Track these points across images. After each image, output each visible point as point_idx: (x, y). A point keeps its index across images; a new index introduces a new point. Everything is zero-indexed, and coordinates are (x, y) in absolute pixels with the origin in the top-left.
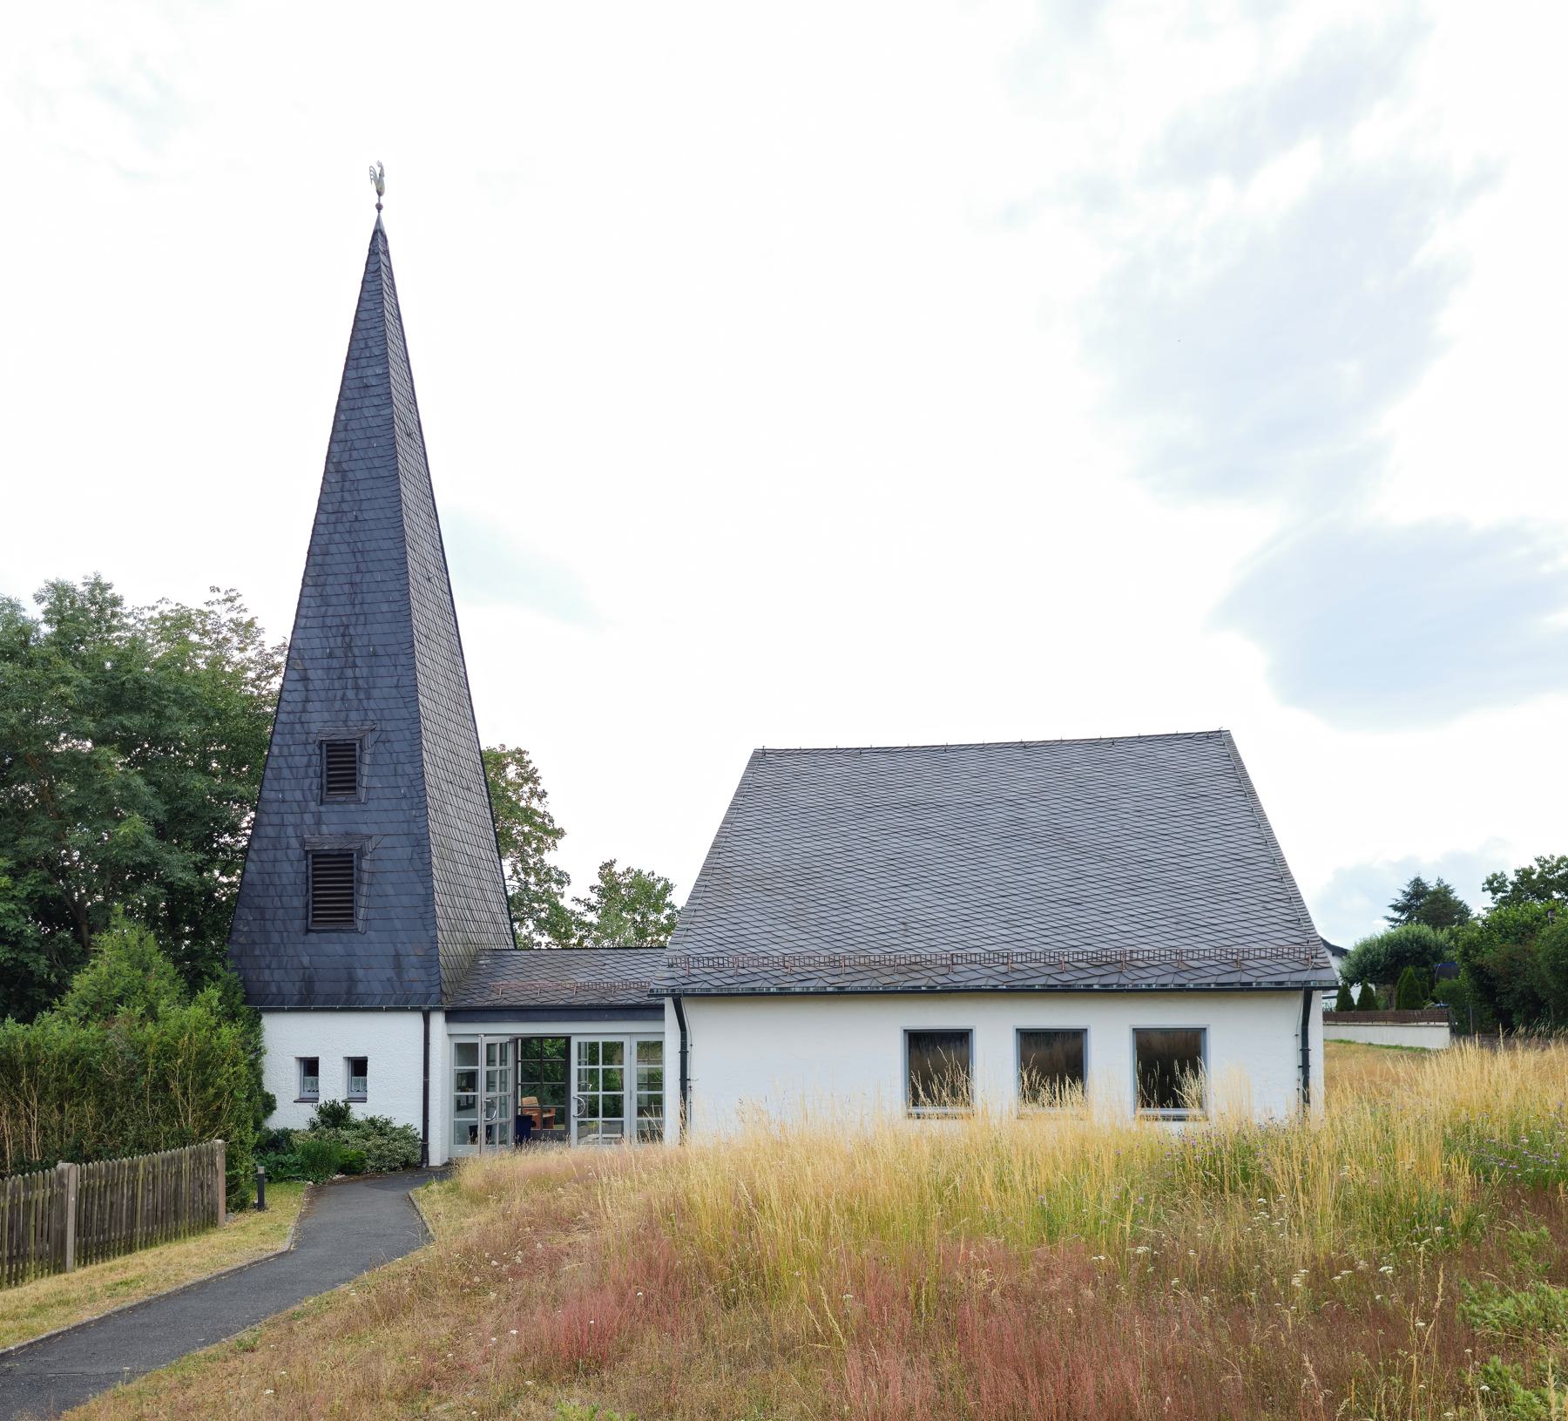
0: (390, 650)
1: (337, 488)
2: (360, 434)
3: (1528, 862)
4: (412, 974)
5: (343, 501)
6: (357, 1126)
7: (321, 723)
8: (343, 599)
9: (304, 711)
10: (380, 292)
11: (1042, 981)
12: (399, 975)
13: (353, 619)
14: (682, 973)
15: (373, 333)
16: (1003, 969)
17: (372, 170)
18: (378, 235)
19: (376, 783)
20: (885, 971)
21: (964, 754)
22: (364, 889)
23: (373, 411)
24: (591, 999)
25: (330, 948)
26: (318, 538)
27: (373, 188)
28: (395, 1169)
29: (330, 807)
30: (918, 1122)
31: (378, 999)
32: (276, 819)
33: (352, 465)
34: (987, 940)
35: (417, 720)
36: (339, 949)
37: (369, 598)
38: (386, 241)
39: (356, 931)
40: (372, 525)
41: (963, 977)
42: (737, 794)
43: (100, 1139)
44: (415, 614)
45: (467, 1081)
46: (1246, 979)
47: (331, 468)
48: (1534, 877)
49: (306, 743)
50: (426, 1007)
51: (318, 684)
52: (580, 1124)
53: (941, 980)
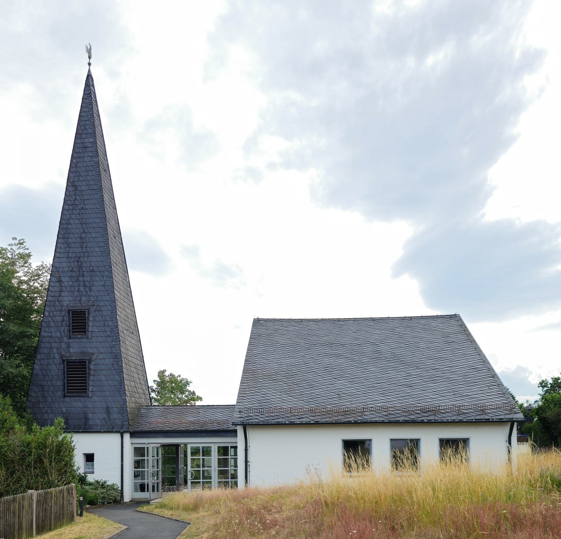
1: (72, 193)
2: (83, 169)
4: (115, 416)
6: (91, 484)
7: (68, 301)
8: (77, 245)
9: (60, 296)
10: (91, 104)
11: (403, 418)
12: (109, 417)
13: (82, 254)
14: (246, 415)
15: (88, 123)
17: (87, 47)
18: (89, 77)
19: (95, 329)
21: (347, 322)
22: (91, 378)
23: (89, 159)
24: (215, 427)
25: (76, 404)
26: (64, 216)
27: (87, 55)
28: (109, 503)
29: (73, 340)
31: (99, 427)
32: (48, 345)
33: (80, 183)
35: (114, 301)
38: (93, 80)
39: (88, 396)
40: (90, 211)
41: (368, 417)
42: (251, 338)
43: (8, 485)
44: (111, 253)
46: (487, 417)
47: (70, 184)
50: (122, 431)
51: (66, 284)
52: (192, 483)
53: (360, 418)
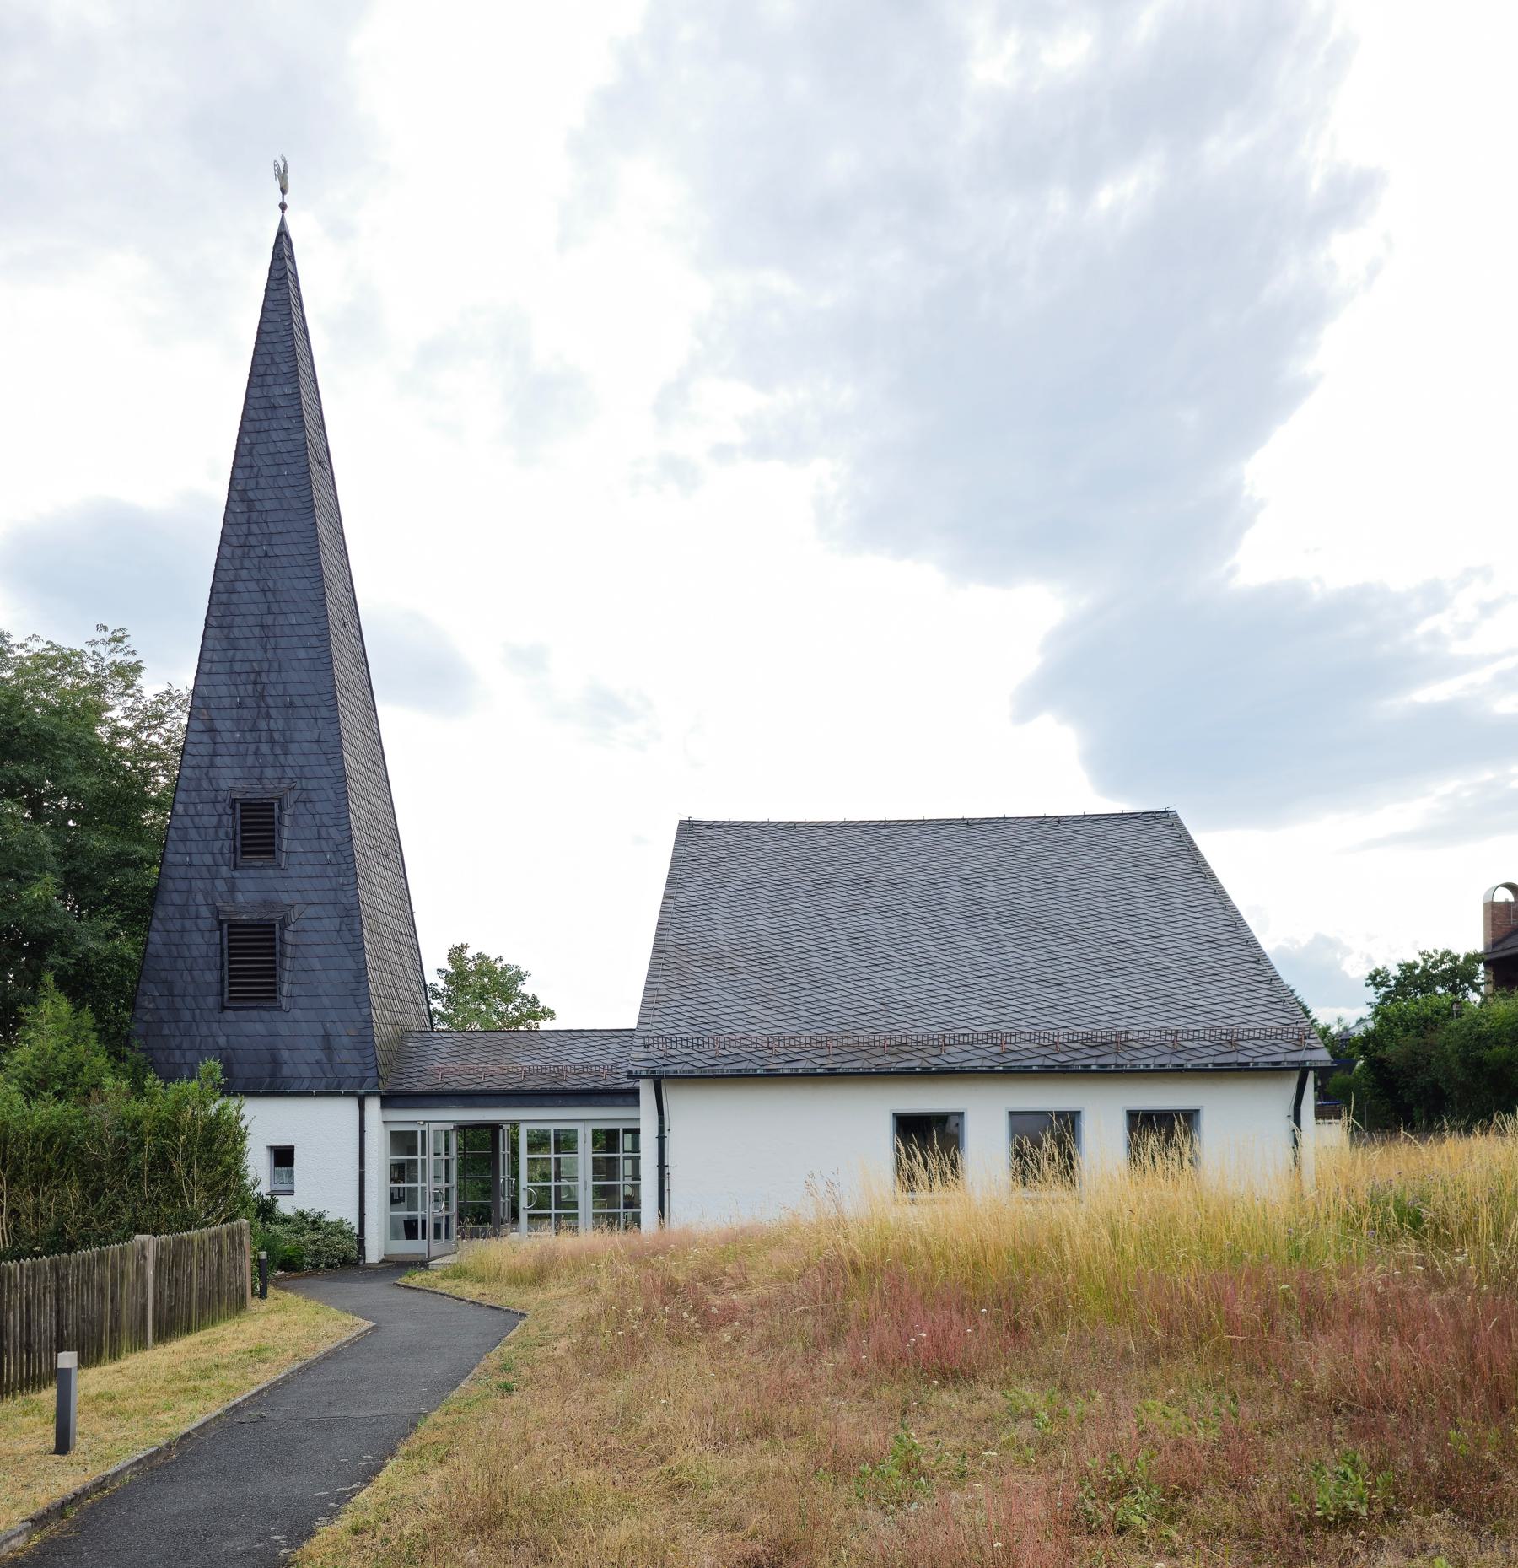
0: (308, 700)
1: (242, 518)
3: (1413, 957)
4: (345, 1056)
5: (250, 533)
6: (286, 1220)
7: (231, 778)
9: (212, 765)
10: (288, 302)
11: (1039, 1061)
13: (266, 665)
14: (660, 1054)
15: (279, 348)
16: (996, 1050)
17: (276, 165)
20: (874, 1052)
22: (288, 963)
23: (282, 435)
24: (542, 1084)
25: (250, 1027)
26: (222, 574)
28: (329, 1266)
30: (915, 1209)
31: (306, 1083)
32: (183, 885)
33: (260, 494)
34: (974, 1019)
36: (260, 1028)
37: (283, 643)
38: (290, 245)
39: (280, 1009)
42: (672, 868)
44: (336, 663)
45: (400, 1172)
46: (1242, 1059)
47: (235, 496)
48: (1417, 971)
49: (215, 802)
50: (362, 1091)
51: (227, 737)
52: (530, 1217)
53: (936, 1061)
